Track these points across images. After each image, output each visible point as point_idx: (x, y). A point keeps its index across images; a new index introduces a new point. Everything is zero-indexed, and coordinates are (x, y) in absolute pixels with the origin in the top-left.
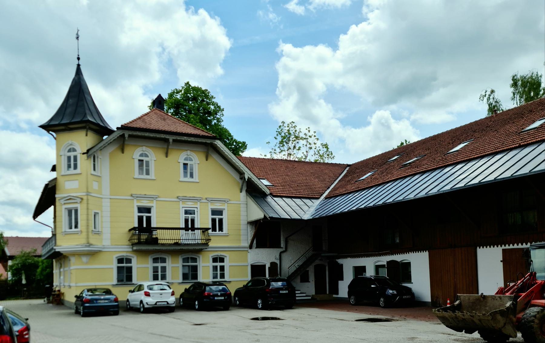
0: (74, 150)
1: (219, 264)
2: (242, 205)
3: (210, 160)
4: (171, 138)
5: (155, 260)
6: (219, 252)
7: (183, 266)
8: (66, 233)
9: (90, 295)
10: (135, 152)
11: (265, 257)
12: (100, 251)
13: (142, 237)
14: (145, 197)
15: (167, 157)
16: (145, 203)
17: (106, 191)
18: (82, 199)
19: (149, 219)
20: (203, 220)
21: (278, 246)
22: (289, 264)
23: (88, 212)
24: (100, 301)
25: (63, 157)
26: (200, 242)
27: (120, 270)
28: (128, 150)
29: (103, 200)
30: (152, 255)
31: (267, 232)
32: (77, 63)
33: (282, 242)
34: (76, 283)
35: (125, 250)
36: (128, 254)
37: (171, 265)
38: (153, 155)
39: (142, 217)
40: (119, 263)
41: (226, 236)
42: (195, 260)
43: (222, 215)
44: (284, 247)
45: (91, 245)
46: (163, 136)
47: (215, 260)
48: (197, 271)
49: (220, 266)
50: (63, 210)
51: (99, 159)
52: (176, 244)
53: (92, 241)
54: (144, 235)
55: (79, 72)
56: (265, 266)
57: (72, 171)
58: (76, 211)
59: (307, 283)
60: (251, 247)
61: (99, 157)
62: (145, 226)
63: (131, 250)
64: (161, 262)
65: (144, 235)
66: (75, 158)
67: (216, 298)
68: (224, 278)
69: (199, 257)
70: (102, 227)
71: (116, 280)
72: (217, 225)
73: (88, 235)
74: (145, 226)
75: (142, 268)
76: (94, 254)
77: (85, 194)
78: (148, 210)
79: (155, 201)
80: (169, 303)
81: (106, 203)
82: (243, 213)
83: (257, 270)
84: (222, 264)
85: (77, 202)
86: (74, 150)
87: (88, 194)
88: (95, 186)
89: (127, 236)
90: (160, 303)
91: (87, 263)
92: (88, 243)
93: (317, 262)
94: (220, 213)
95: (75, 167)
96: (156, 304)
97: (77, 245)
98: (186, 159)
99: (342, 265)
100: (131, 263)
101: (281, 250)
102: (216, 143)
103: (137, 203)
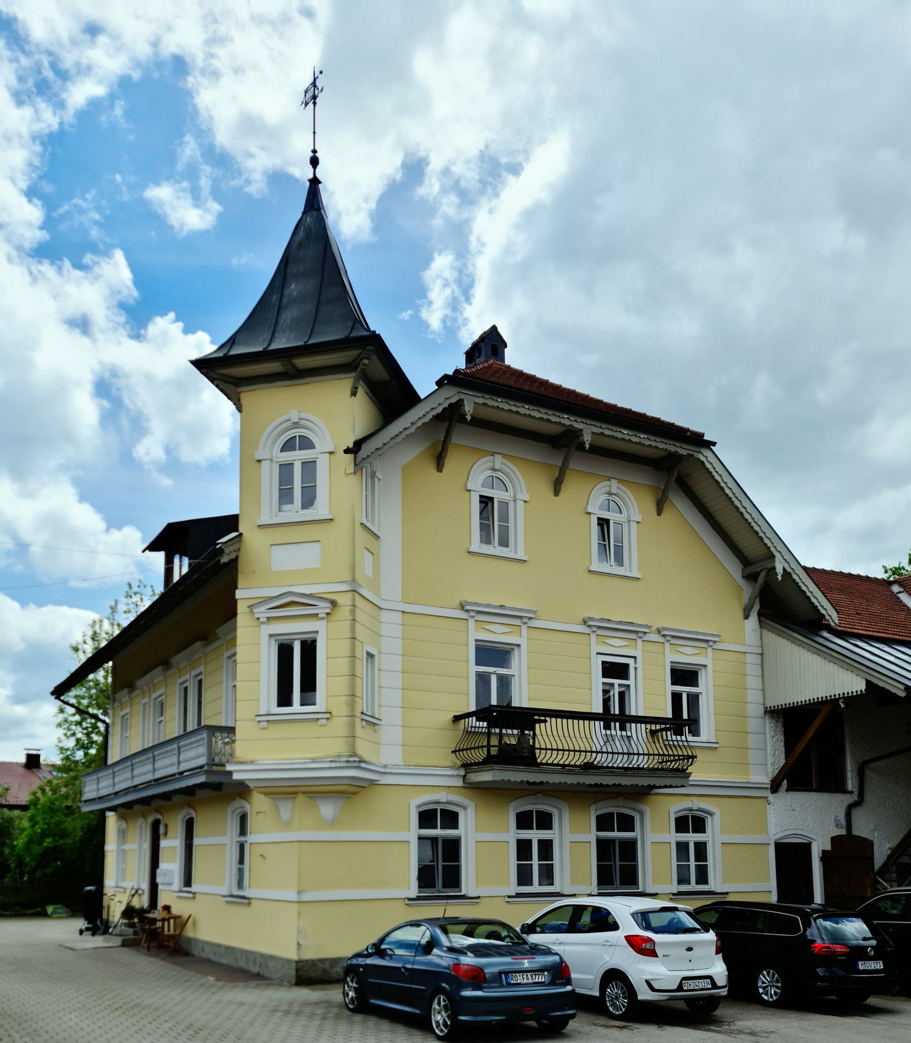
0: (306, 444)
1: (692, 838)
4: (589, 431)
5: (523, 821)
7: (420, 838)
8: (270, 721)
9: (477, 950)
10: (479, 471)
11: (814, 820)
15: (557, 492)
17: (391, 590)
18: (334, 603)
19: (505, 683)
24: (520, 979)
25: (265, 465)
26: (643, 762)
32: (311, 176)
33: (849, 775)
34: (299, 892)
35: (440, 784)
36: (442, 796)
37: (569, 837)
42: (627, 823)
43: (695, 684)
44: (856, 792)
47: (682, 824)
48: (634, 857)
49: (540, 842)
50: (265, 639)
52: (588, 767)
53: (363, 750)
54: (501, 736)
57: (294, 511)
58: (309, 648)
60: (775, 787)
61: (379, 474)
63: (459, 783)
64: (539, 828)
65: (501, 736)
66: (309, 467)
69: (642, 814)
71: (414, 883)
72: (682, 720)
73: (352, 726)
75: (487, 843)
76: (355, 793)
77: (345, 587)
81: (392, 625)
82: (753, 682)
83: (791, 858)
86: (306, 444)
88: (366, 563)
89: (451, 739)
91: (332, 824)
92: (354, 755)
95: (309, 500)
96: (680, 988)
97: (314, 761)
103: (476, 633)
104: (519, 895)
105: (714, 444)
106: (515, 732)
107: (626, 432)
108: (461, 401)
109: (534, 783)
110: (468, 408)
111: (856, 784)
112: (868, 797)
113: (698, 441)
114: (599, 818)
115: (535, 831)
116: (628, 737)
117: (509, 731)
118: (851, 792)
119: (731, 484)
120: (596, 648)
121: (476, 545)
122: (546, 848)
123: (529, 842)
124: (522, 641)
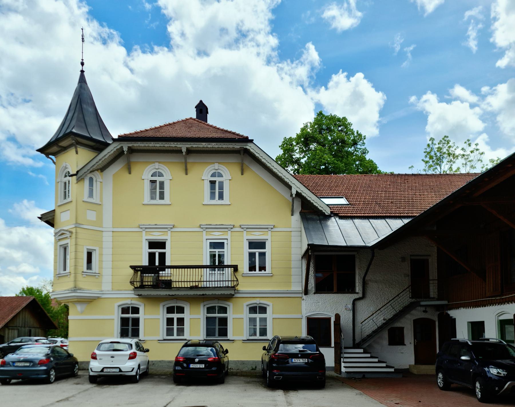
2: (293, 234)
3: (247, 174)
5: (170, 310)
6: (258, 299)
10: (145, 171)
11: (330, 306)
12: (98, 298)
13: (145, 279)
14: (156, 227)
15: (187, 174)
16: (157, 236)
18: (71, 232)
19: (162, 256)
20: (237, 254)
21: (352, 291)
22: (371, 314)
23: (76, 248)
27: (124, 322)
28: (135, 170)
29: (104, 233)
30: (205, 303)
31: (331, 269)
35: (129, 297)
36: (128, 302)
38: (169, 172)
39: (154, 254)
40: (122, 313)
41: (271, 276)
42: (224, 310)
45: (80, 289)
46: (173, 145)
47: (253, 310)
48: (226, 324)
51: (98, 183)
53: (80, 285)
54: (152, 275)
55: (82, 79)
56: (329, 319)
59: (400, 347)
62: (157, 264)
67: (192, 366)
68: (266, 335)
70: (101, 268)
72: (257, 263)
73: (75, 277)
74: (157, 264)
76: (91, 302)
77: (74, 226)
78: (162, 245)
79: (169, 232)
80: (123, 370)
84: (180, 316)
85: (67, 237)
87: (77, 225)
90: (109, 370)
91: (82, 313)
93: (417, 314)
94: (261, 245)
96: (102, 371)
97: (65, 290)
98: (213, 175)
99: (455, 319)
100: (138, 313)
101: (356, 296)
102: (248, 148)
104: (248, 340)
105: (253, 140)
106: (153, 275)
107: (204, 144)
108: (122, 147)
109: (172, 295)
110: (125, 149)
111: (361, 289)
112: (369, 294)
113: (246, 140)
114: (168, 308)
115: (175, 314)
116: (223, 274)
117: (147, 275)
118: (358, 293)
119: (265, 156)
120: (205, 237)
121: (207, 200)
122: (181, 321)
123: (173, 319)
124: (228, 237)
